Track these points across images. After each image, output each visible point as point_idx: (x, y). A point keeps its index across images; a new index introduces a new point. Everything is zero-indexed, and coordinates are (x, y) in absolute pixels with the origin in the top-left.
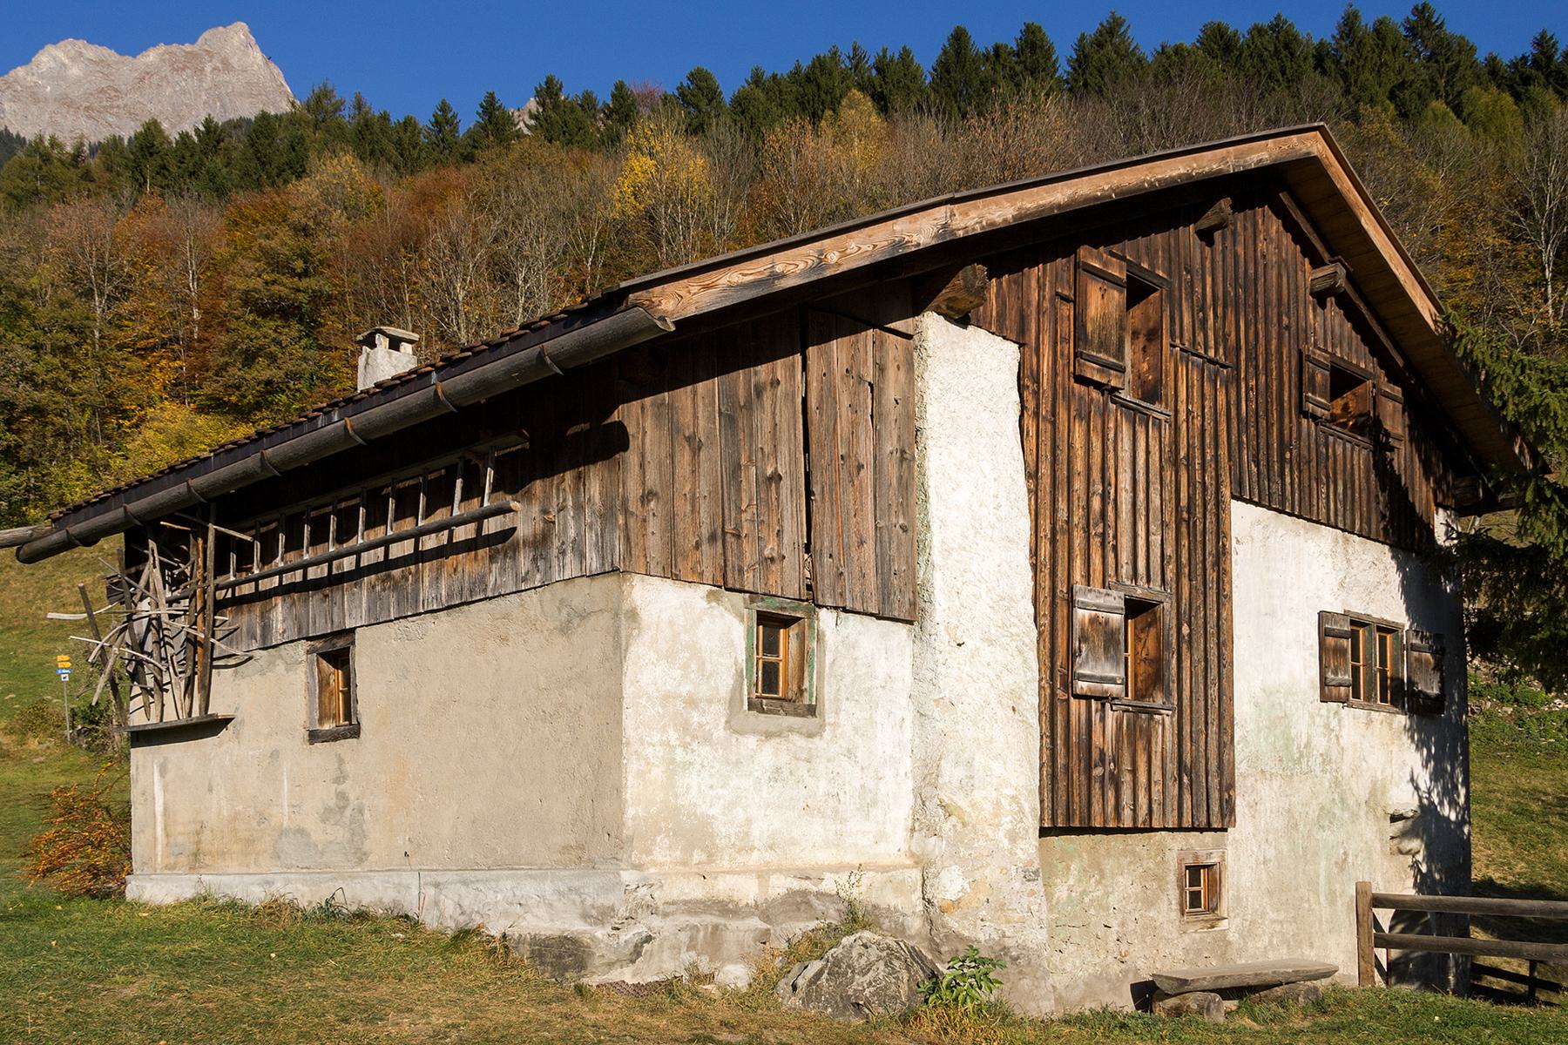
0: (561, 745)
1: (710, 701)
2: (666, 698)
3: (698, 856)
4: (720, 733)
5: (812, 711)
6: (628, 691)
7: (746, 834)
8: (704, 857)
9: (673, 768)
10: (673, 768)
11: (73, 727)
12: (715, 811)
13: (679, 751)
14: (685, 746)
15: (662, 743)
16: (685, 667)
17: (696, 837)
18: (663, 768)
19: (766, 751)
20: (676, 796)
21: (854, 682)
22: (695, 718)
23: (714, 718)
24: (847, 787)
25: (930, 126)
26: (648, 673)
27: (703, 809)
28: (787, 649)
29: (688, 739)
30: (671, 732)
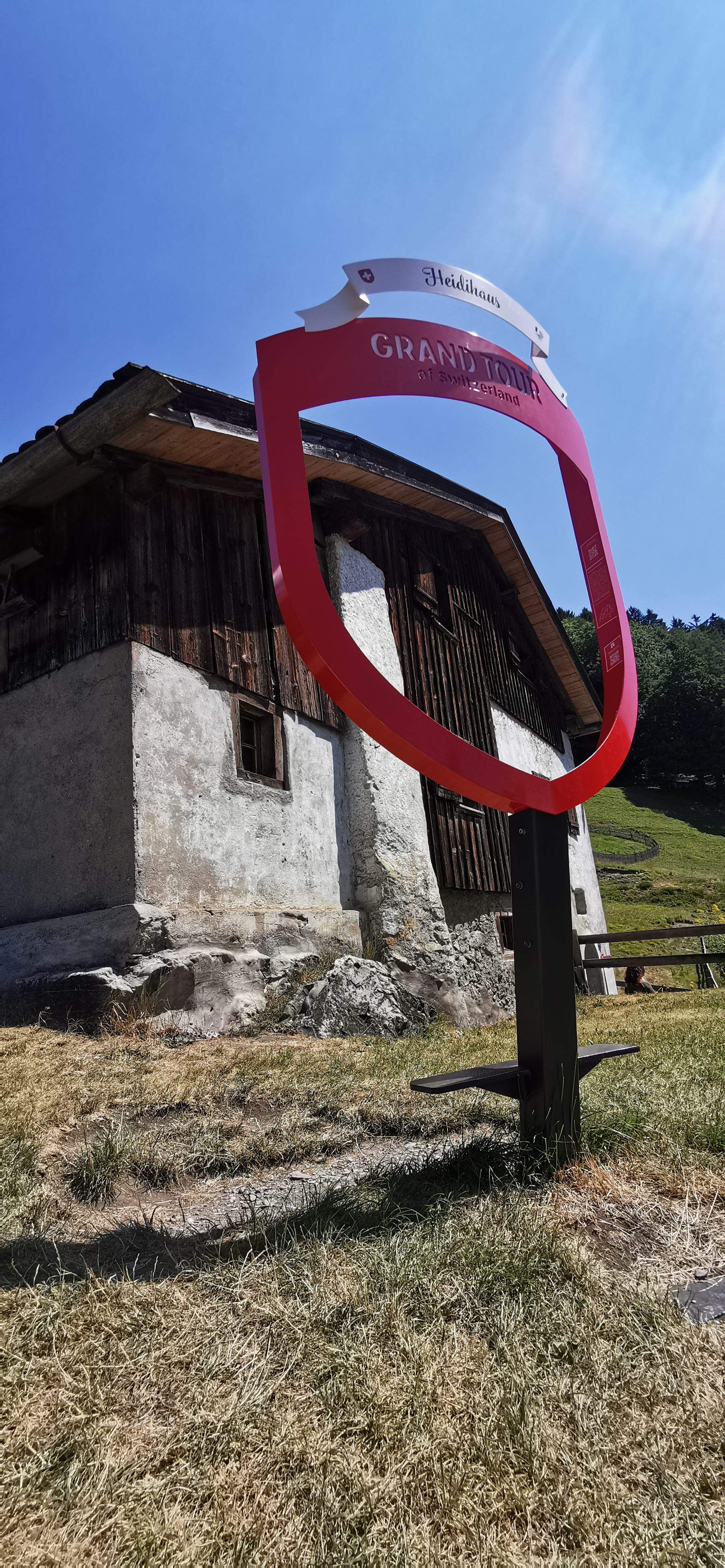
0: (71, 802)
1: (207, 763)
2: (170, 755)
3: (202, 897)
4: (216, 791)
5: (285, 785)
6: (137, 742)
7: (242, 879)
8: (208, 897)
9: (179, 816)
10: (179, 816)
11: (522, 1435)
12: (217, 856)
13: (183, 801)
14: (188, 797)
15: (169, 793)
16: (186, 731)
17: (201, 877)
18: (169, 814)
19: (252, 808)
20: (182, 841)
21: (309, 769)
22: (196, 775)
23: (211, 779)
24: (311, 847)
25: (227, 693)
26: (150, 730)
27: (206, 854)
28: (259, 739)
29: (191, 792)
30: (176, 783)
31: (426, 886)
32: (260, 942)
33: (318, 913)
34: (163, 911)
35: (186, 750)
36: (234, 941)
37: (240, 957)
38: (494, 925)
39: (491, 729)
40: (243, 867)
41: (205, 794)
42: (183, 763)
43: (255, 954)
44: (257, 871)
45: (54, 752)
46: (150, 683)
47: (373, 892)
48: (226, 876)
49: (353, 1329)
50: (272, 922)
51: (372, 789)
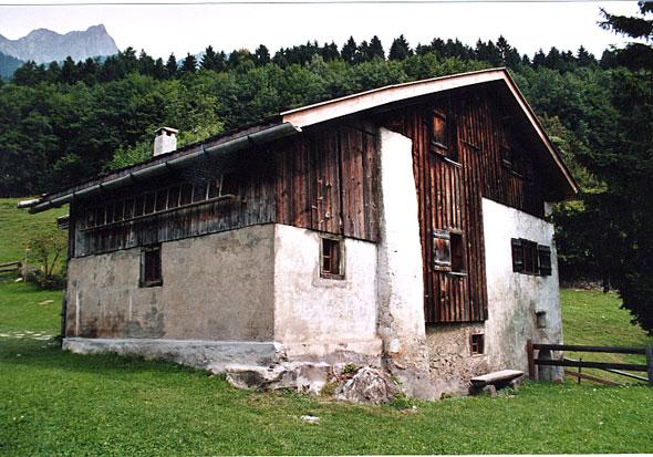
6: (276, 270)
17: (301, 329)
19: (330, 291)
26: (283, 264)
27: (304, 318)
31: (417, 327)
32: (326, 358)
33: (354, 341)
34: (286, 345)
35: (297, 269)
36: (314, 358)
37: (316, 365)
38: (467, 340)
39: (480, 209)
40: (320, 323)
41: (304, 290)
42: (295, 277)
43: (324, 364)
44: (326, 324)
45: (240, 266)
46: (283, 241)
47: (387, 331)
48: (312, 327)
49: (239, 114)
50: (333, 347)
51: (391, 275)
